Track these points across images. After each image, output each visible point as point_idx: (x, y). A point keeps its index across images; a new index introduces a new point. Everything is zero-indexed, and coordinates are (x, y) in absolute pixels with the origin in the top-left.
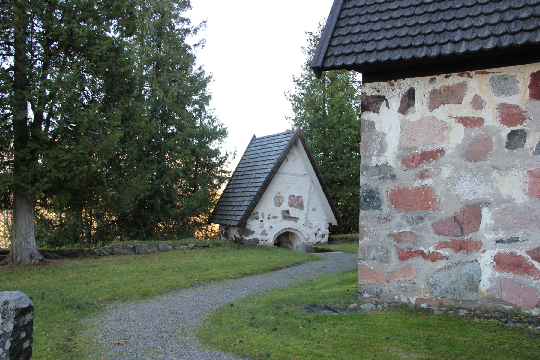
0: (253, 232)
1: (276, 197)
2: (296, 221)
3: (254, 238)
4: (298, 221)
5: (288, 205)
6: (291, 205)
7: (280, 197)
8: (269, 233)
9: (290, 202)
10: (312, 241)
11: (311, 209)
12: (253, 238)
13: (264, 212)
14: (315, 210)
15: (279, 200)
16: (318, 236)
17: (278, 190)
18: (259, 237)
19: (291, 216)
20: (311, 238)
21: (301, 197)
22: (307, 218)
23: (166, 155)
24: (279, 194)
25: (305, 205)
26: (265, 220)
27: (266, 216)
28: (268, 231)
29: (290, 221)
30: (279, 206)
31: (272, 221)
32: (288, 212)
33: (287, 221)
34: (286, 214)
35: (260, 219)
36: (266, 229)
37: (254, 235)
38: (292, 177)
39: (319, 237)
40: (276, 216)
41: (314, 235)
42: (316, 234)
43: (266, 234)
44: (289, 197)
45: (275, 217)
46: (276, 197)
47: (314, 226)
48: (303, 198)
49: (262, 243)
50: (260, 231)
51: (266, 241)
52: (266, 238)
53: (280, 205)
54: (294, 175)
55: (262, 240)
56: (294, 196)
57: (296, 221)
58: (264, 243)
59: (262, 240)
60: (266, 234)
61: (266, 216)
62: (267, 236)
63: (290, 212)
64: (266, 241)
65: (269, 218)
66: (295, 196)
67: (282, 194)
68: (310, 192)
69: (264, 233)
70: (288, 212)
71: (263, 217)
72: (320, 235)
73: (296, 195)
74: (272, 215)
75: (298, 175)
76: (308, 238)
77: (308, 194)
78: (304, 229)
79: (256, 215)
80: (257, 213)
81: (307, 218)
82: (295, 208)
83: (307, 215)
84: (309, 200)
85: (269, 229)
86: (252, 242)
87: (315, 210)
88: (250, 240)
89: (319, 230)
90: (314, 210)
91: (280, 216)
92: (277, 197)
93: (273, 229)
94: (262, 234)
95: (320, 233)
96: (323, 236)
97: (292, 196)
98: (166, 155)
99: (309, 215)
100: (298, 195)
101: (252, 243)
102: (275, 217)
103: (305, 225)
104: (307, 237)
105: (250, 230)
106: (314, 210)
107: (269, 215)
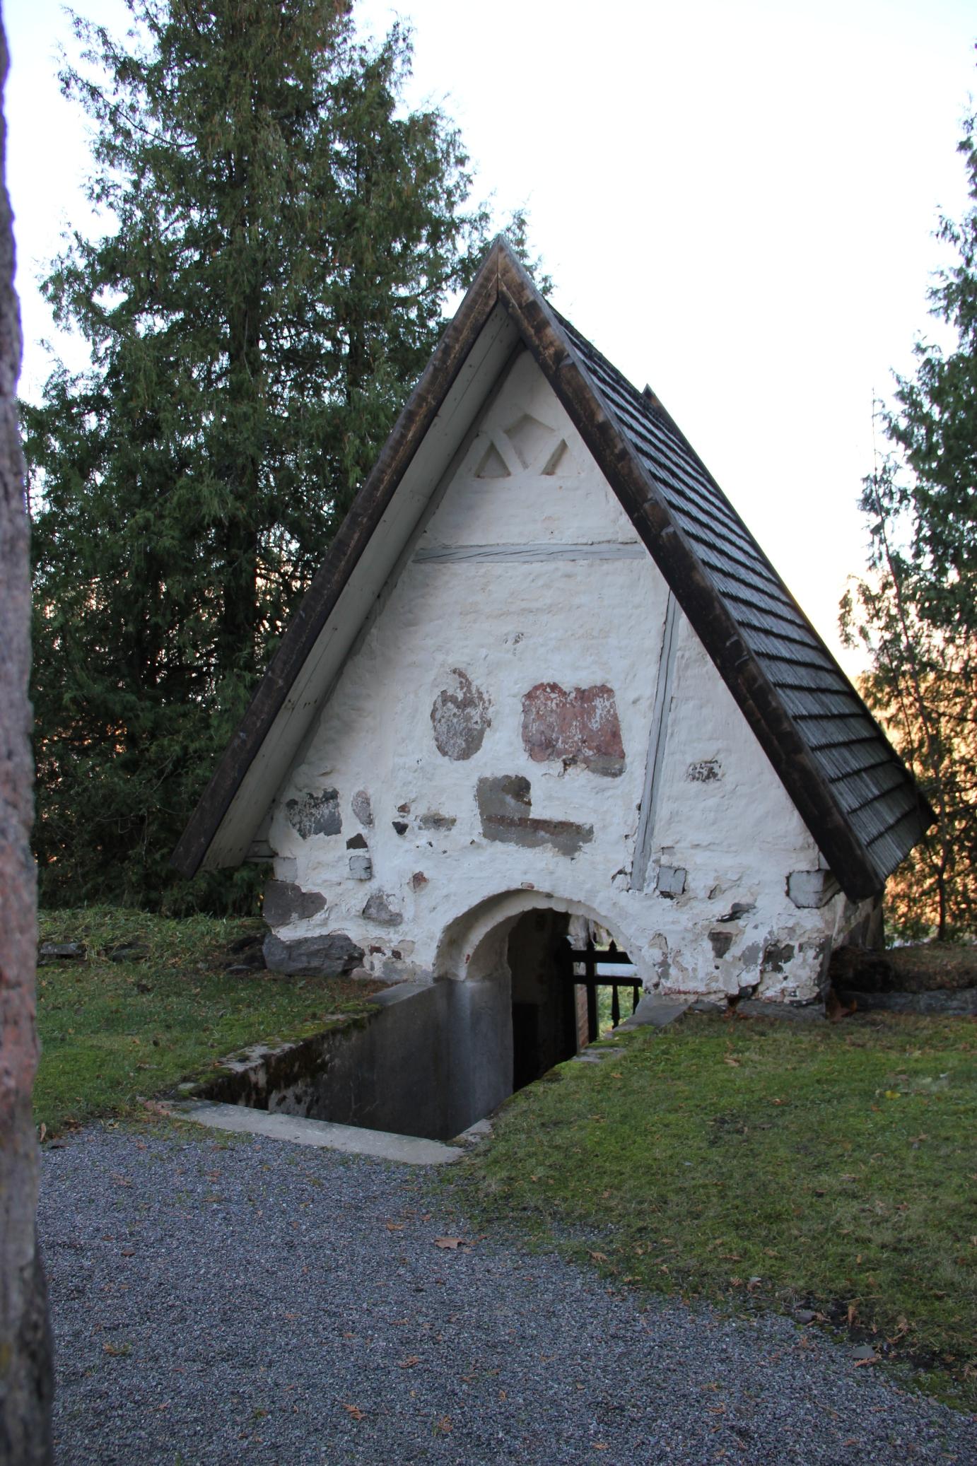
0: (312, 903)
1: (445, 698)
2: (569, 850)
3: (325, 932)
4: (586, 847)
5: (520, 744)
6: (541, 747)
7: (467, 703)
8: (408, 914)
9: (534, 727)
10: (691, 985)
11: (682, 770)
12: (316, 933)
13: (370, 792)
14: (711, 774)
15: (468, 718)
16: (735, 951)
17: (456, 658)
18: (359, 933)
19: (536, 813)
20: (687, 960)
21: (605, 691)
22: (647, 828)
23: (298, 545)
24: (465, 682)
25: (635, 743)
26: (382, 838)
27: (386, 815)
28: (403, 901)
29: (533, 845)
30: (466, 754)
31: (423, 842)
32: (520, 788)
33: (511, 847)
34: (510, 800)
35: (351, 827)
36: (388, 889)
37: (319, 917)
38: (537, 567)
39: (747, 958)
40: (446, 813)
41: (708, 945)
42: (721, 942)
43: (394, 921)
44: (529, 696)
45: (437, 822)
46: (445, 698)
47: (699, 883)
48: (618, 698)
49: (378, 965)
50: (359, 898)
51: (397, 955)
52: (392, 938)
53: (471, 744)
54: (552, 555)
55: (378, 950)
56: (554, 687)
57: (569, 850)
58: (385, 965)
59: (378, 950)
60: (394, 921)
61: (386, 815)
62: (402, 928)
63: (535, 794)
64: (397, 955)
65: (401, 829)
66: (566, 687)
67: (478, 680)
68: (665, 653)
69: (376, 910)
70: (520, 788)
71: (369, 821)
72: (753, 949)
73: (569, 681)
74: (419, 810)
75: (574, 553)
76: (664, 964)
77: (650, 670)
78: (631, 902)
79: (325, 810)
80: (332, 796)
81: (647, 828)
82: (566, 764)
83: (647, 809)
84: (664, 706)
85: (407, 891)
86: (315, 954)
87: (711, 774)
88: (300, 943)
89: (736, 913)
90: (707, 773)
91: (467, 812)
92: (453, 699)
93: (430, 896)
94: (365, 913)
95: (751, 934)
96: (775, 956)
97: (541, 687)
98: (298, 545)
99: (663, 810)
100: (586, 679)
101: (315, 963)
102: (437, 822)
103: (633, 877)
104: (657, 955)
105: (297, 889)
106: (707, 773)
107: (403, 809)
